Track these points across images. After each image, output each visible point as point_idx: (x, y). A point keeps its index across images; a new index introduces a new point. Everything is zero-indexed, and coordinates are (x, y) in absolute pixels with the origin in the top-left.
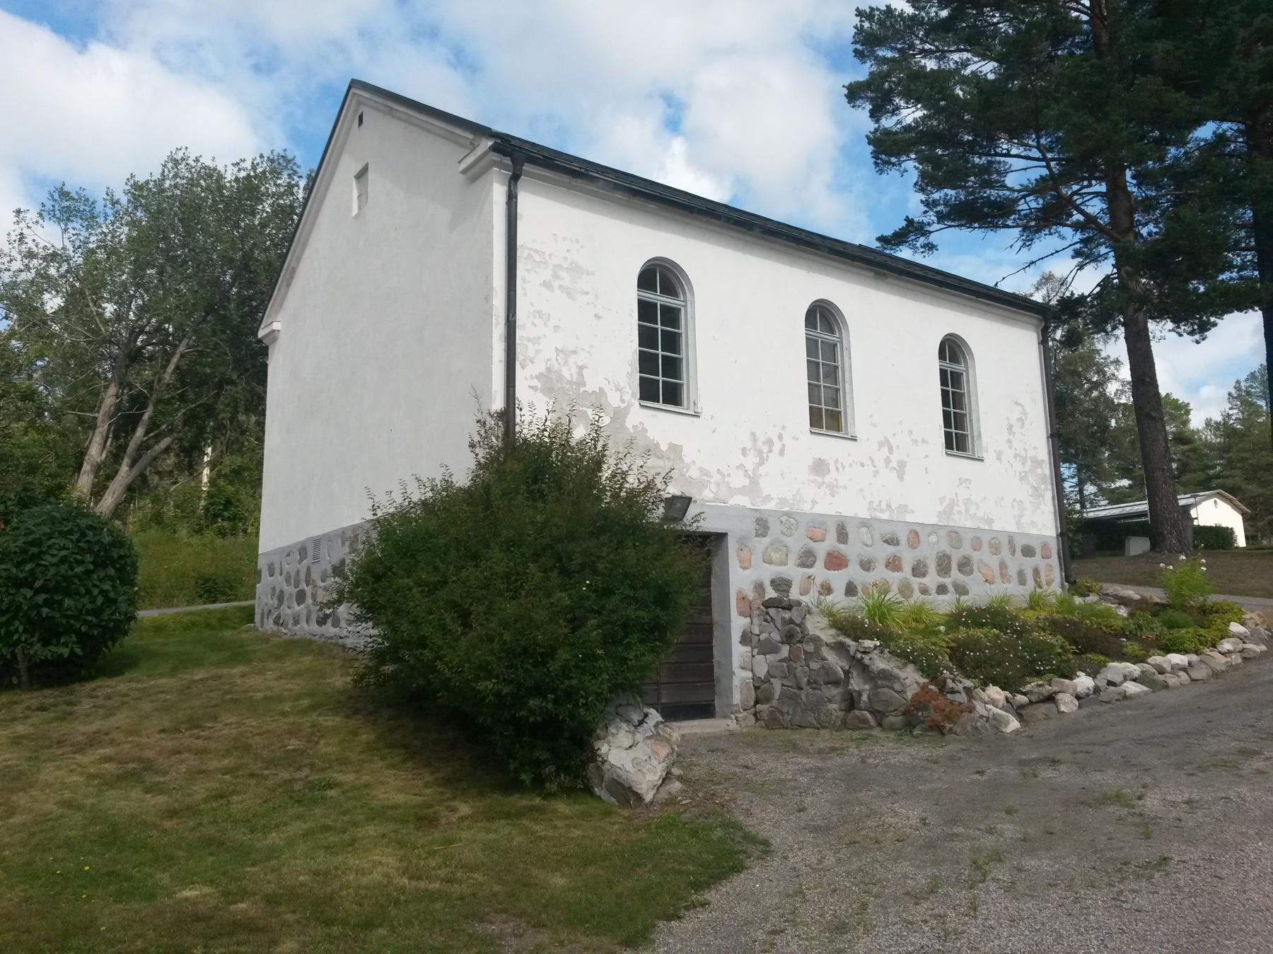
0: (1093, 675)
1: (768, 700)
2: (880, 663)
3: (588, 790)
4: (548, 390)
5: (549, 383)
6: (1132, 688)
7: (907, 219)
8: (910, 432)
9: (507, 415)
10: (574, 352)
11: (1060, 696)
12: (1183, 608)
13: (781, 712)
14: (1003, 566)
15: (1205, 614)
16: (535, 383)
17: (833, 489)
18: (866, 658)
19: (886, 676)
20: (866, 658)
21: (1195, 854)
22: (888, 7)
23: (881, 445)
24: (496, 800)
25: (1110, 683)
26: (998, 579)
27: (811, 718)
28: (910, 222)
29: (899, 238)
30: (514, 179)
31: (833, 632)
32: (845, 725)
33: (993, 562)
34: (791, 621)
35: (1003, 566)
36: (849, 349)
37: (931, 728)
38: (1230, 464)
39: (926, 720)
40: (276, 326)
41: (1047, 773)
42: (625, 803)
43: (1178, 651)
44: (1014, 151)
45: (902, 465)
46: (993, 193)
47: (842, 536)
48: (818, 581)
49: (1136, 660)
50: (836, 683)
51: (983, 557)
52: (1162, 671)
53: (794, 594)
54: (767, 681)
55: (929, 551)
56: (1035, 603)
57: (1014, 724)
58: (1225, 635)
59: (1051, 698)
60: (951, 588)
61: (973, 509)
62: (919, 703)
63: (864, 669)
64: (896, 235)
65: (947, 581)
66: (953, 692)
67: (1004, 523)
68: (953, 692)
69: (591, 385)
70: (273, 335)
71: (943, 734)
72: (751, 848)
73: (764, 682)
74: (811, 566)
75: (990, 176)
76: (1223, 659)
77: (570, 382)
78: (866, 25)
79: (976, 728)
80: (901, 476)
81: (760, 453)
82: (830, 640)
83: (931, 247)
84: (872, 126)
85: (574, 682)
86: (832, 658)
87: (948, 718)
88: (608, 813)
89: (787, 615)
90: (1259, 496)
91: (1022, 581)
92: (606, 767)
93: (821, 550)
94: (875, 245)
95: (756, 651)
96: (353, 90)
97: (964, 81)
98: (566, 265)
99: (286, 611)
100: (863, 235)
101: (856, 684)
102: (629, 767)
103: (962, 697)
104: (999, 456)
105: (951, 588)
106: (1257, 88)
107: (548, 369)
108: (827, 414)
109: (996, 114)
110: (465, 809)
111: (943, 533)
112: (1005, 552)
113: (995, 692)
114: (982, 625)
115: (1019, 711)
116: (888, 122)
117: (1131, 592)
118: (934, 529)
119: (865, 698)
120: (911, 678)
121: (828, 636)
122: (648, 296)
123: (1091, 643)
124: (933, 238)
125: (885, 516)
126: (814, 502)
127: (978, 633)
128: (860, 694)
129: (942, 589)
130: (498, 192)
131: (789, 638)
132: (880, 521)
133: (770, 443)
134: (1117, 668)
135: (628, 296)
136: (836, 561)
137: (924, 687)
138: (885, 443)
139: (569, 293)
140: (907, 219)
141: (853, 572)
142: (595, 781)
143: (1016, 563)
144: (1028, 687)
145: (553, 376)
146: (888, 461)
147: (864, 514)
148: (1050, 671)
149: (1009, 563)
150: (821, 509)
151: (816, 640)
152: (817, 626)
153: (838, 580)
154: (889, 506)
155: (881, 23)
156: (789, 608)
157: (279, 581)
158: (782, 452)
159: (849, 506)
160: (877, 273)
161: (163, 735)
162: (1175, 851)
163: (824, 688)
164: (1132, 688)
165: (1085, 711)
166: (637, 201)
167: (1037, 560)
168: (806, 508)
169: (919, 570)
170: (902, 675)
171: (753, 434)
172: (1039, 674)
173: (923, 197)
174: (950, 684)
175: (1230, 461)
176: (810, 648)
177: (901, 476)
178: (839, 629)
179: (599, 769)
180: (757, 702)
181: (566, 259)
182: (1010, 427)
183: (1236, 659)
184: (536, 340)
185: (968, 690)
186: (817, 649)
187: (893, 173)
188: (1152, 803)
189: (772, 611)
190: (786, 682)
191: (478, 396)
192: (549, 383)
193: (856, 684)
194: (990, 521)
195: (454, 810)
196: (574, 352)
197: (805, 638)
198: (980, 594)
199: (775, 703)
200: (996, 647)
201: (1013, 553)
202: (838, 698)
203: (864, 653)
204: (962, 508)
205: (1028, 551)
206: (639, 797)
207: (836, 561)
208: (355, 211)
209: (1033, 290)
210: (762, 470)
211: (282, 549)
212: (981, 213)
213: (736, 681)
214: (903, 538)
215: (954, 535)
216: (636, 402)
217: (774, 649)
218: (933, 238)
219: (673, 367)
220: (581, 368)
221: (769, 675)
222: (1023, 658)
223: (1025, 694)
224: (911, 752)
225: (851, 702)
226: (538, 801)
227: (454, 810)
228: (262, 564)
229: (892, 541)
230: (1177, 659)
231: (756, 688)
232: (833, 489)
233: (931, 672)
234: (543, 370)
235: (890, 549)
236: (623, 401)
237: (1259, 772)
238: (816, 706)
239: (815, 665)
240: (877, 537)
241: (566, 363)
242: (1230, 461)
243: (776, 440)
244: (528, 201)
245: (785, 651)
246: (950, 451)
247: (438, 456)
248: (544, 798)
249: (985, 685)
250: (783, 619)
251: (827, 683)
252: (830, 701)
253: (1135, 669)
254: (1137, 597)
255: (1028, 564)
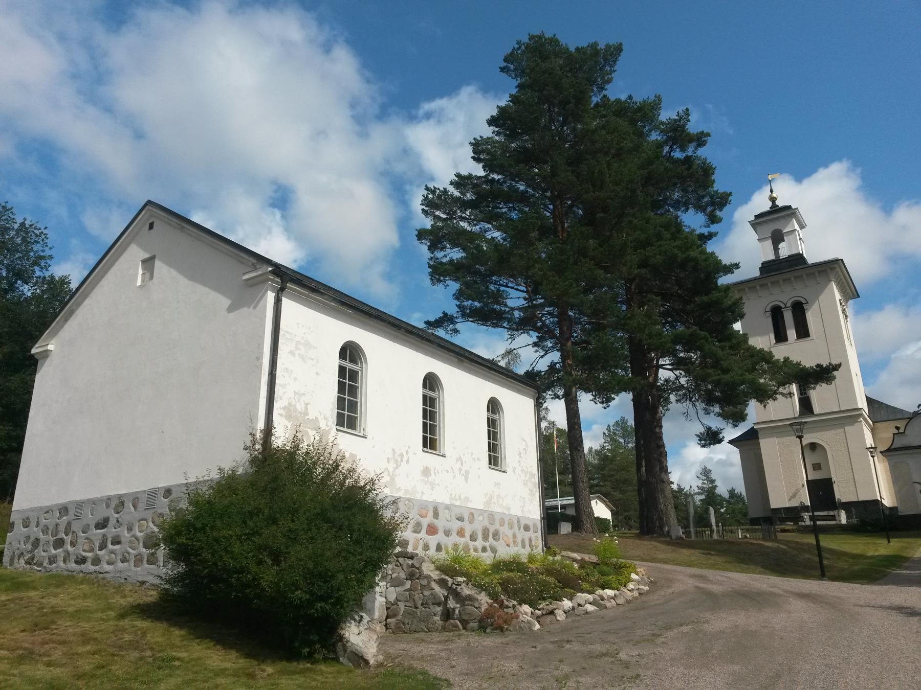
0: (571, 599)
1: (394, 616)
2: (466, 591)
3: (336, 660)
4: (289, 417)
5: (289, 413)
6: (590, 608)
7: (444, 313)
8: (472, 454)
9: (268, 431)
10: (304, 394)
11: (556, 611)
12: (606, 564)
13: (404, 624)
14: (514, 536)
15: (619, 569)
16: (282, 412)
17: (433, 486)
18: (459, 588)
19: (470, 598)
20: (459, 588)
21: (649, 673)
22: (445, 189)
23: (457, 460)
24: (284, 664)
25: (579, 605)
26: (512, 544)
27: (423, 625)
28: (445, 314)
29: (438, 323)
30: (282, 289)
31: (438, 572)
32: (444, 629)
33: (510, 534)
34: (413, 566)
35: (514, 536)
36: (443, 402)
37: (496, 629)
38: (604, 478)
39: (488, 624)
40: (50, 347)
41: (568, 646)
42: (358, 666)
43: (609, 588)
44: (510, 285)
45: (467, 472)
46: (497, 307)
47: (436, 515)
48: (532, 531)
49: (590, 592)
50: (439, 604)
51: (505, 530)
52: (603, 599)
53: (410, 549)
54: (395, 603)
55: (478, 526)
56: (531, 559)
57: (537, 626)
58: (630, 580)
59: (552, 613)
60: (489, 549)
61: (501, 501)
62: (488, 614)
63: (457, 595)
64: (436, 321)
65: (487, 544)
66: (507, 607)
67: (516, 511)
68: (507, 607)
69: (311, 416)
70: (46, 354)
71: (502, 631)
72: (441, 683)
73: (393, 605)
74: (419, 532)
75: (498, 297)
76: (630, 594)
77: (300, 413)
78: (431, 196)
79: (521, 627)
80: (466, 479)
81: (396, 461)
82: (436, 578)
83: (456, 331)
84: (430, 255)
85: (343, 593)
86: (437, 589)
87: (505, 622)
88: (350, 671)
89: (410, 562)
90: (620, 499)
91: (524, 547)
92: (349, 644)
93: (425, 522)
94: (421, 325)
95: (389, 585)
96: (148, 207)
97: (487, 241)
98: (303, 341)
99: (40, 553)
100: (417, 320)
101: (452, 604)
102: (361, 644)
103: (511, 611)
104: (514, 469)
105: (489, 549)
106: (636, 272)
107: (289, 404)
108: (430, 442)
109: (503, 262)
110: (270, 670)
111: (486, 515)
112: (516, 528)
113: (526, 608)
114: (512, 571)
115: (538, 618)
116: (439, 254)
117: (577, 556)
118: (482, 512)
119: (457, 612)
120: (484, 600)
121: (435, 575)
122: (344, 363)
123: (568, 584)
124: (458, 326)
125: (458, 503)
126: (423, 493)
127: (512, 575)
128: (454, 610)
129: (484, 549)
130: (271, 296)
131: (411, 577)
132: (455, 506)
133: (402, 455)
134: (582, 597)
135: (334, 362)
136: (432, 530)
137: (490, 605)
138: (459, 459)
139: (303, 358)
140: (444, 313)
141: (440, 537)
142: (341, 653)
143: (521, 535)
144: (541, 606)
145: (292, 408)
146: (460, 470)
147: (448, 502)
148: (549, 598)
149: (518, 535)
150: (425, 498)
151: (428, 577)
152: (428, 569)
153: (433, 541)
154: (460, 497)
155: (439, 197)
156: (412, 558)
157: (35, 532)
158: (408, 462)
159: (440, 496)
160: (459, 360)
161: (24, 634)
162: (641, 672)
163: (432, 607)
164: (590, 608)
165: (570, 620)
166: (343, 308)
167: (530, 534)
168: (418, 496)
169: (473, 538)
170: (480, 598)
171: (393, 450)
172: (544, 599)
173: (458, 303)
174: (506, 603)
175: (603, 475)
176: (424, 582)
177: (466, 479)
178: (441, 571)
179: (344, 646)
180: (387, 617)
181: (303, 338)
182: (520, 454)
183: (636, 594)
184: (284, 386)
185: (514, 606)
186: (429, 583)
187: (441, 286)
188: (623, 655)
189: (401, 560)
190: (408, 604)
191: (253, 419)
192: (289, 413)
193: (452, 604)
194: (509, 509)
195: (264, 671)
196: (304, 394)
197: (421, 576)
198: (505, 552)
199: (399, 617)
200: (517, 583)
201: (519, 529)
202: (440, 613)
203: (458, 585)
204: (495, 501)
205: (527, 528)
206: (366, 662)
207: (432, 530)
208: (139, 283)
209: (500, 358)
210: (397, 472)
211: (41, 508)
212: (489, 315)
213: (377, 604)
214: (466, 518)
215: (491, 516)
216: (334, 427)
217: (401, 584)
218: (458, 326)
219: (353, 407)
220: (307, 404)
221: (397, 600)
222: (536, 589)
223: (539, 610)
224: (490, 641)
225: (447, 615)
226: (309, 665)
227: (264, 671)
228: (13, 517)
229: (460, 519)
230: (609, 592)
231: (388, 609)
232: (433, 486)
233: (494, 596)
234: (287, 404)
235: (459, 524)
236: (327, 426)
237: (663, 643)
238: (426, 619)
239: (427, 593)
240: (454, 518)
241: (299, 401)
242: (603, 475)
243: (405, 454)
244: (287, 304)
245: (408, 584)
246: (492, 466)
247: (202, 454)
248: (312, 664)
249: (520, 604)
250: (408, 564)
251: (433, 604)
252: (435, 615)
253: (590, 597)
254: (579, 558)
255: (527, 535)
